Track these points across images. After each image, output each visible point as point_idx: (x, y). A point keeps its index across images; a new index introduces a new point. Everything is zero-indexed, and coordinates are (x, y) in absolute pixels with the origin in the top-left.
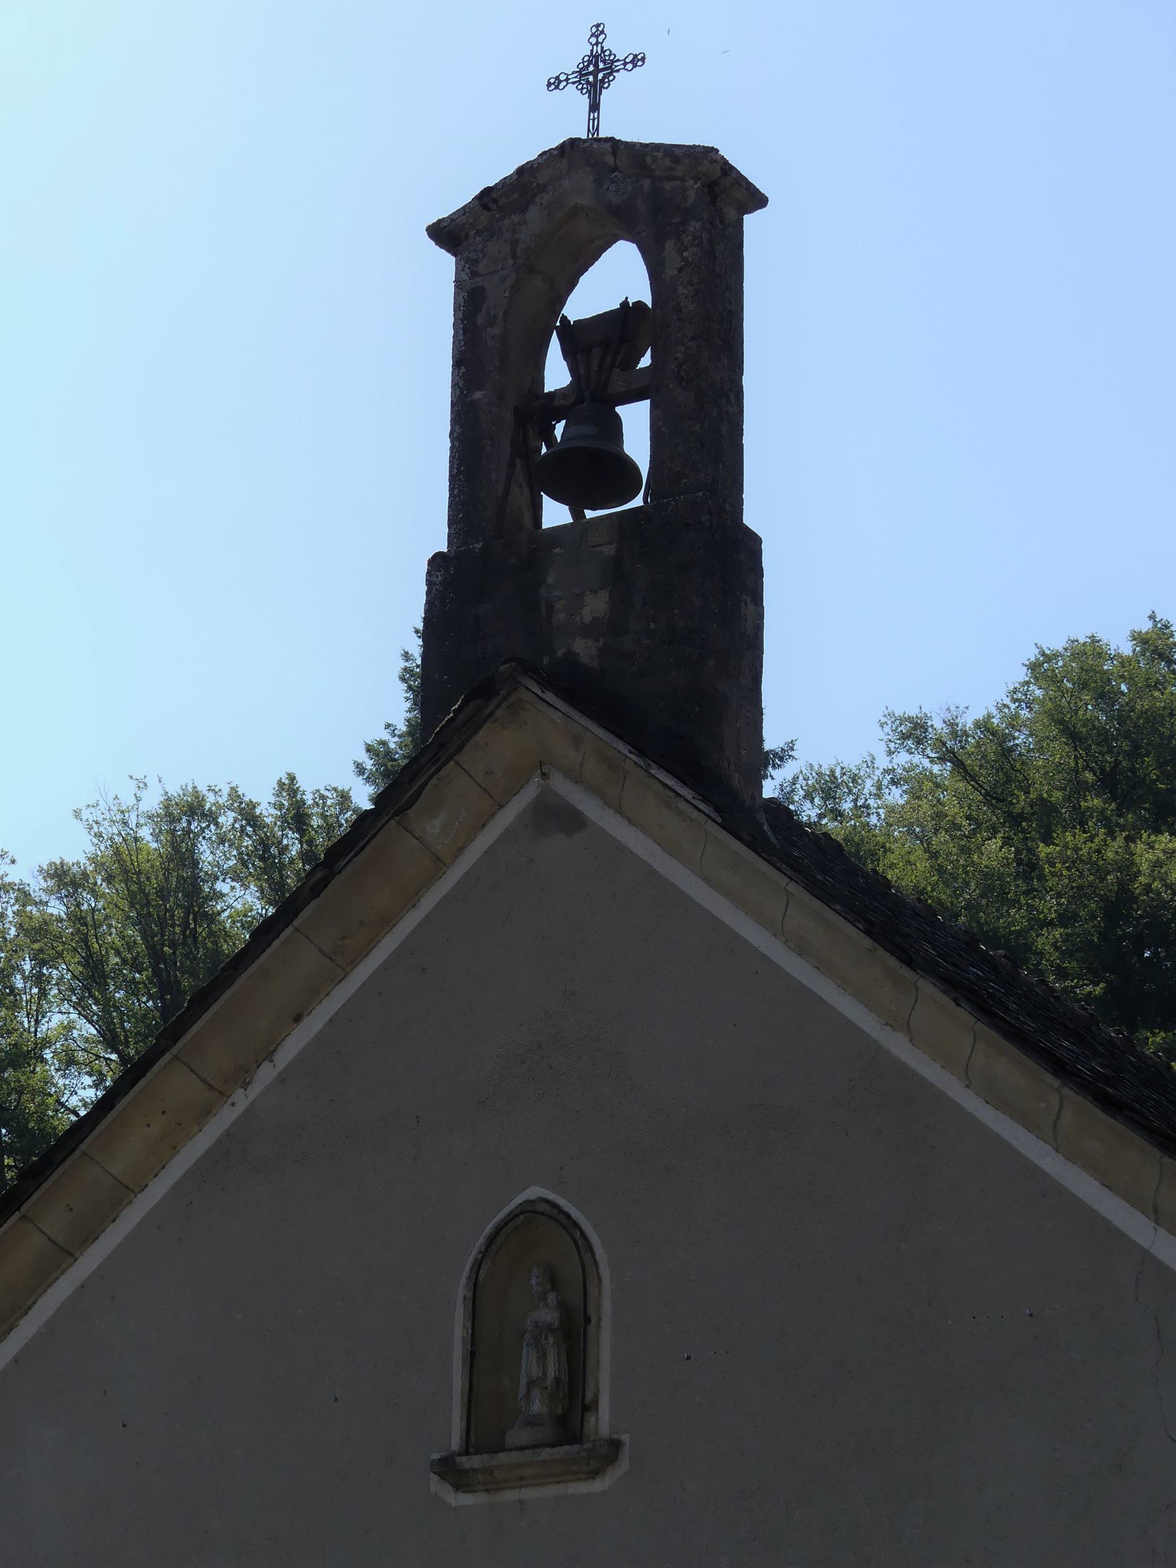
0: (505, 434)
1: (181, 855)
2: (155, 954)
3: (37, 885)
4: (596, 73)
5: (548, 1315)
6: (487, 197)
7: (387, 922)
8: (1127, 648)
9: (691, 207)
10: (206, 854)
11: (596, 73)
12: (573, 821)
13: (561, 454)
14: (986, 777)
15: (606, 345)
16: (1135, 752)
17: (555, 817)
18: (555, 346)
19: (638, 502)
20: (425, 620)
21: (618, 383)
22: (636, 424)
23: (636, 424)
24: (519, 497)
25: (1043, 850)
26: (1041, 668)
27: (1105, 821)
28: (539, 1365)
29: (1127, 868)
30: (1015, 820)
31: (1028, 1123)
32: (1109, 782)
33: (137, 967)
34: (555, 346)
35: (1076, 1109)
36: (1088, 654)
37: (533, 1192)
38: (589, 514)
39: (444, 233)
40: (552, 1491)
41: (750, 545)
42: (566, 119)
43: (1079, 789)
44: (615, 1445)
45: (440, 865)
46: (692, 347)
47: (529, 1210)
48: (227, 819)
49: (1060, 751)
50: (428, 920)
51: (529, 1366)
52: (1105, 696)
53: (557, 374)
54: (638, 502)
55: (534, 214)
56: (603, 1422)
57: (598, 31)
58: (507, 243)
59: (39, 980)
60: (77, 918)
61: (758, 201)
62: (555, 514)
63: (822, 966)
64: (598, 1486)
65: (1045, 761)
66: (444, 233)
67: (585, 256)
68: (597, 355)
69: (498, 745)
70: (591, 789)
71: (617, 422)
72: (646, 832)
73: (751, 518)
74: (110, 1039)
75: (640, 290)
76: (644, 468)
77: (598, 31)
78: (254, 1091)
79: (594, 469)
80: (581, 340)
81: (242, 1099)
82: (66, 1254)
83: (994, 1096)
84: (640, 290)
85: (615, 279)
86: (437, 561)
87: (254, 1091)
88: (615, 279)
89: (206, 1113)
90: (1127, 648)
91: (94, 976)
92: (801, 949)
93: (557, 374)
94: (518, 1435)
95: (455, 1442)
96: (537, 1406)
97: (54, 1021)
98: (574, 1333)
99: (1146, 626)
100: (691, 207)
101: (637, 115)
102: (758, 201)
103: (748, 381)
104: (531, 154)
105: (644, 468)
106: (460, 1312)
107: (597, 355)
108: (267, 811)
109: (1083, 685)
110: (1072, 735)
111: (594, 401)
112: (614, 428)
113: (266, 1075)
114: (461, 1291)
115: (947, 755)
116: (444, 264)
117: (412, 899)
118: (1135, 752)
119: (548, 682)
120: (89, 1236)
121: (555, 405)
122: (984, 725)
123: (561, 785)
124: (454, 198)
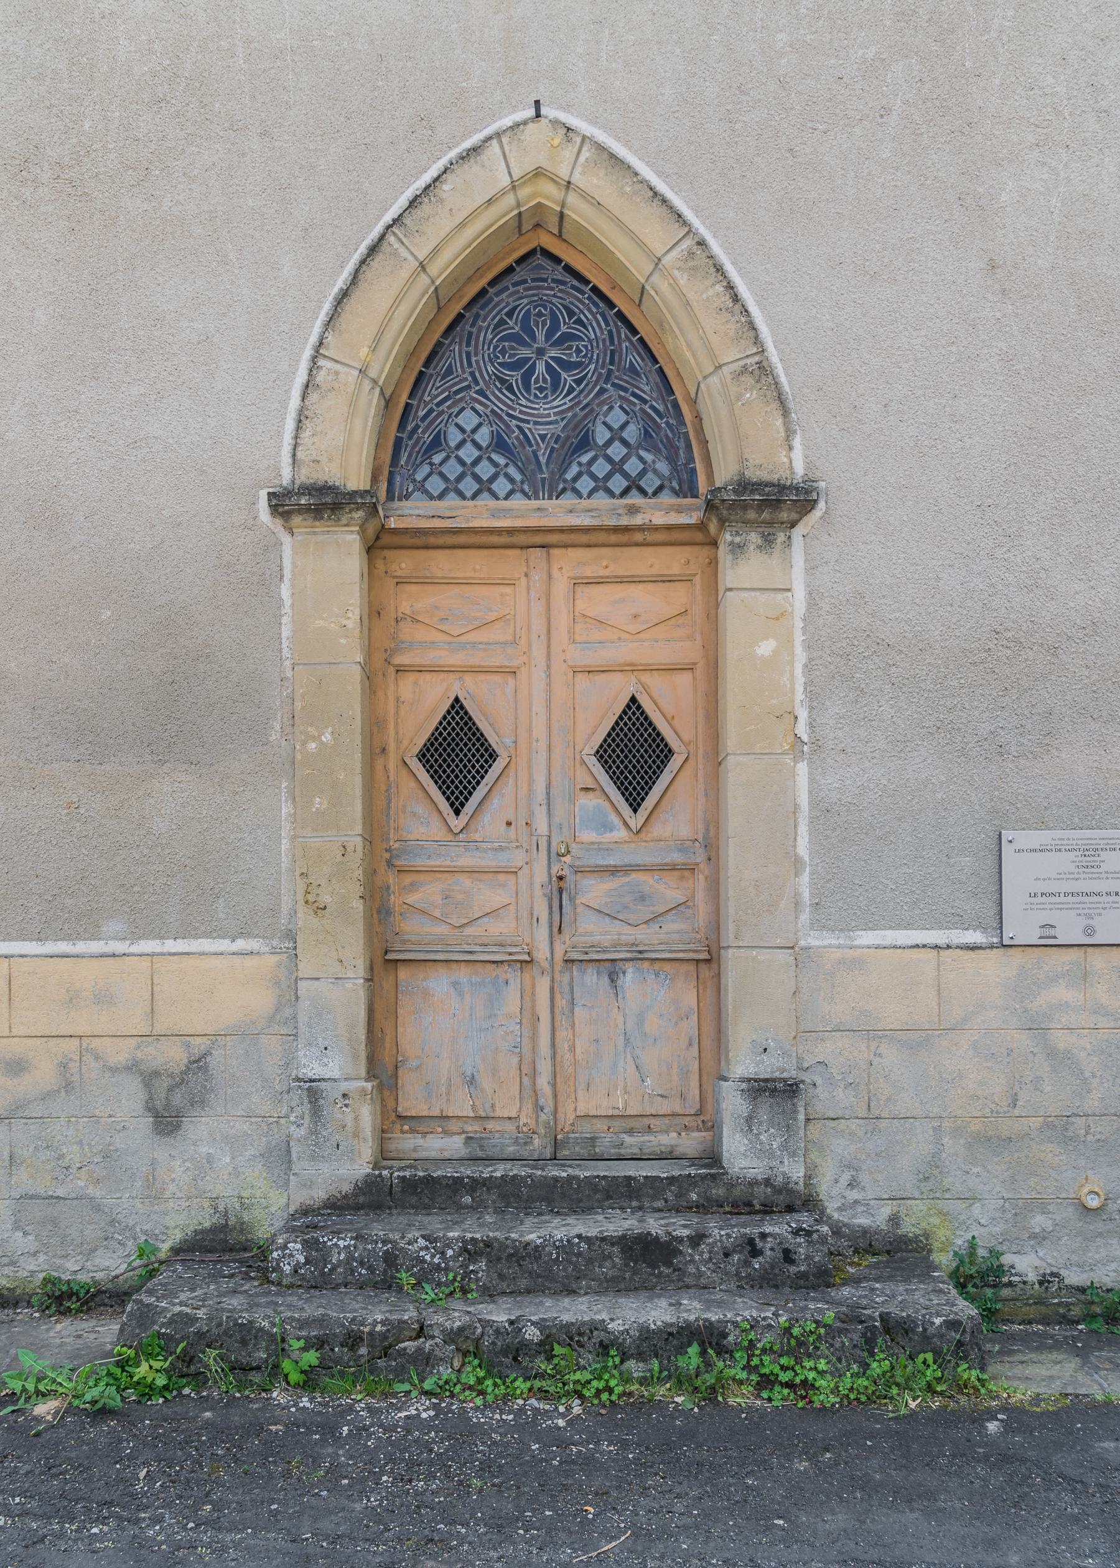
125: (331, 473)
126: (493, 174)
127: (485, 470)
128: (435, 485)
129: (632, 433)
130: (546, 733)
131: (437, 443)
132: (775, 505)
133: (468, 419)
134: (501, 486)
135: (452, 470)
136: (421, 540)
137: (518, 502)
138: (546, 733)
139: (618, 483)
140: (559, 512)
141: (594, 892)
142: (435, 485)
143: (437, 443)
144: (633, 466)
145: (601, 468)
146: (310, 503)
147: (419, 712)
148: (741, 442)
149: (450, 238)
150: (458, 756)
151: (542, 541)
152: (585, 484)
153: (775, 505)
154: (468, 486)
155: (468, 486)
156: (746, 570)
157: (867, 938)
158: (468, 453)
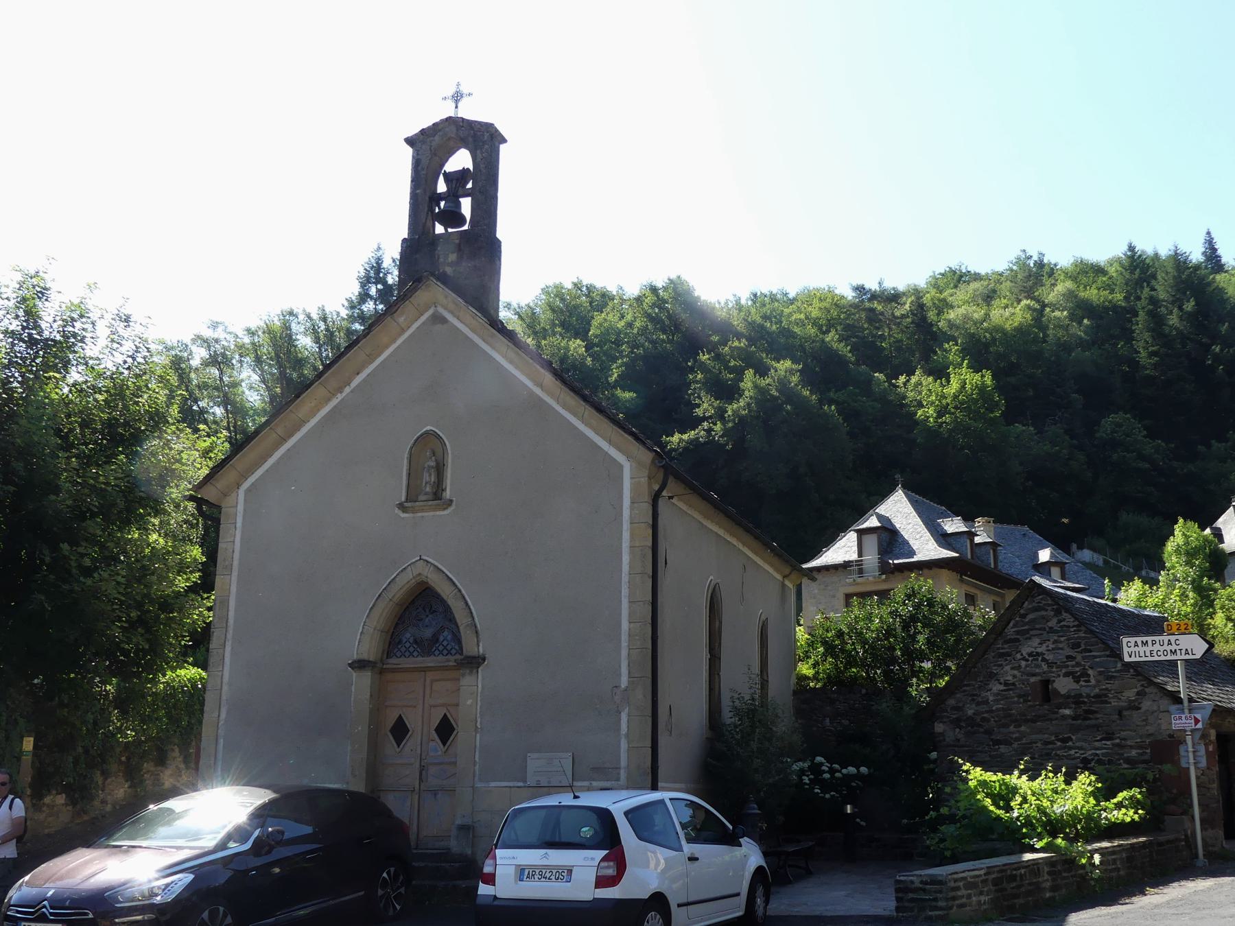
0: (424, 203)
1: (286, 327)
2: (277, 356)
3: (241, 333)
4: (457, 97)
5: (433, 464)
6: (423, 132)
7: (387, 347)
8: (570, 286)
9: (484, 140)
10: (294, 327)
11: (457, 97)
12: (444, 321)
13: (441, 211)
14: (528, 321)
15: (458, 179)
16: (571, 316)
17: (438, 319)
18: (441, 178)
19: (466, 227)
20: (402, 254)
21: (461, 191)
22: (466, 205)
23: (466, 205)
24: (429, 223)
25: (543, 342)
26: (545, 291)
27: (561, 335)
28: (429, 478)
29: (567, 349)
30: (535, 333)
31: (575, 415)
32: (563, 325)
33: (271, 359)
34: (441, 178)
35: (589, 411)
36: (559, 287)
37: (429, 428)
38: (450, 230)
39: (410, 141)
40: (432, 513)
41: (499, 243)
42: (447, 111)
43: (554, 325)
44: (451, 501)
45: (403, 331)
46: (484, 181)
47: (427, 433)
48: (301, 317)
49: (549, 315)
50: (398, 347)
51: (426, 477)
52: (563, 300)
53: (442, 187)
54: (466, 227)
55: (437, 138)
56: (447, 494)
57: (458, 84)
58: (430, 145)
59: (241, 362)
60: (253, 344)
61: (504, 141)
62: (439, 229)
63: (517, 367)
64: (446, 512)
65: (545, 317)
66: (410, 141)
67: (451, 152)
68: (455, 182)
69: (422, 296)
70: (452, 312)
71: (459, 203)
72: (464, 322)
73: (499, 235)
74: (264, 381)
75: (469, 165)
76: (468, 217)
77: (458, 84)
78: (344, 394)
79: (453, 217)
80: (448, 177)
81: (340, 397)
82: (284, 440)
83: (564, 406)
84: (469, 165)
85: (461, 160)
86: (404, 240)
87: (344, 394)
88: (461, 160)
89: (329, 400)
90: (570, 286)
91: (258, 360)
92: (511, 362)
93: (442, 187)
94: (422, 497)
95: (403, 499)
96: (428, 489)
97: (244, 375)
98: (440, 469)
99: (576, 281)
100: (484, 140)
101: (470, 111)
102: (504, 141)
103: (499, 195)
104: (437, 120)
105: (468, 217)
106: (406, 462)
107: (455, 182)
108: (315, 316)
109: (556, 296)
110: (553, 310)
111: (454, 195)
112: (459, 205)
113: (347, 390)
114: (406, 455)
115: (517, 313)
116: (409, 151)
117: (394, 341)
118: (571, 316)
119: (438, 279)
120: (291, 435)
121: (440, 197)
122: (528, 306)
123: (441, 310)
124: (413, 130)
125: (365, 656)
126: (409, 575)
127: (411, 649)
128: (398, 654)
129: (449, 637)
130: (421, 725)
131: (400, 642)
132: (475, 662)
133: (408, 635)
134: (415, 654)
135: (403, 649)
136: (393, 671)
137: (420, 659)
138: (421, 725)
139: (445, 652)
140: (430, 661)
141: (433, 770)
142: (398, 654)
143: (400, 642)
144: (449, 647)
145: (441, 648)
146: (359, 665)
147: (391, 721)
148: (470, 647)
149: (406, 580)
150: (400, 730)
151: (425, 670)
152: (437, 653)
153: (475, 662)
154: (407, 654)
155: (407, 654)
156: (467, 681)
157: (493, 784)
158: (408, 645)
